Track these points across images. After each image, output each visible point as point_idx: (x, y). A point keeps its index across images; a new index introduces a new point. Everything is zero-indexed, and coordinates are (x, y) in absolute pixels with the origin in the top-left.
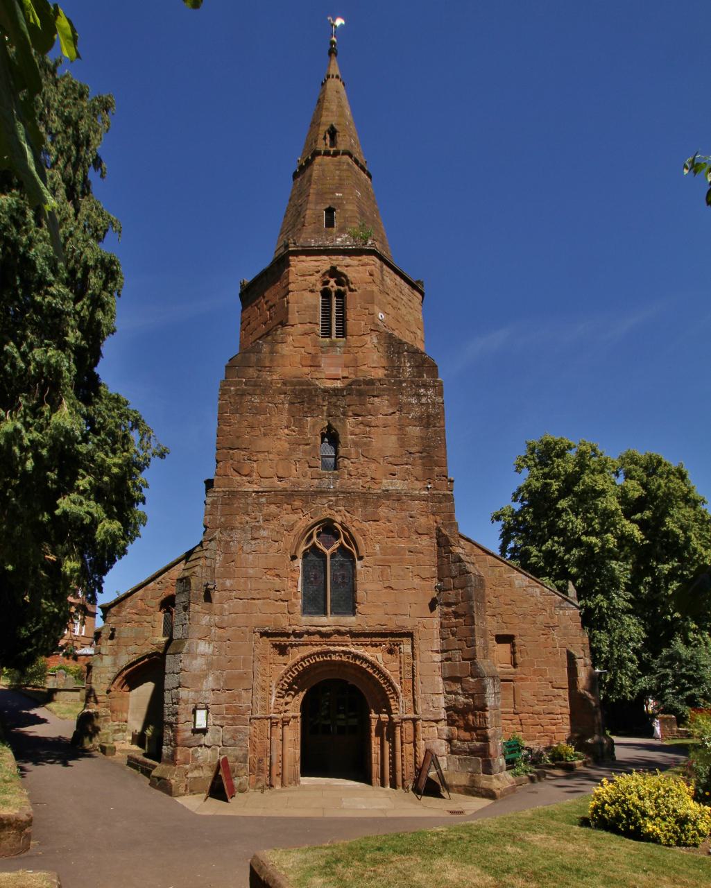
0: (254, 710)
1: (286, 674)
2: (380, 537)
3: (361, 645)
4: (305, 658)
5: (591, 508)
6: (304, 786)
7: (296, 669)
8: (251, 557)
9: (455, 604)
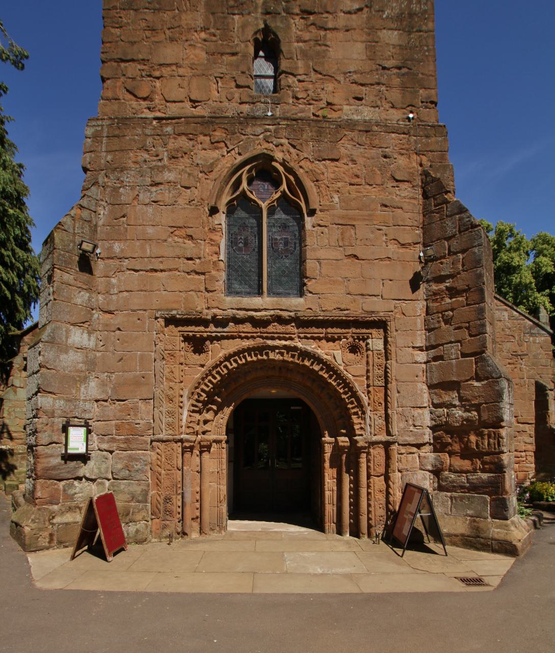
0: (157, 429)
1: (203, 379)
2: (339, 184)
3: (313, 338)
5: (505, 284)
6: (232, 533)
7: (218, 373)
8: (150, 210)
9: (451, 276)
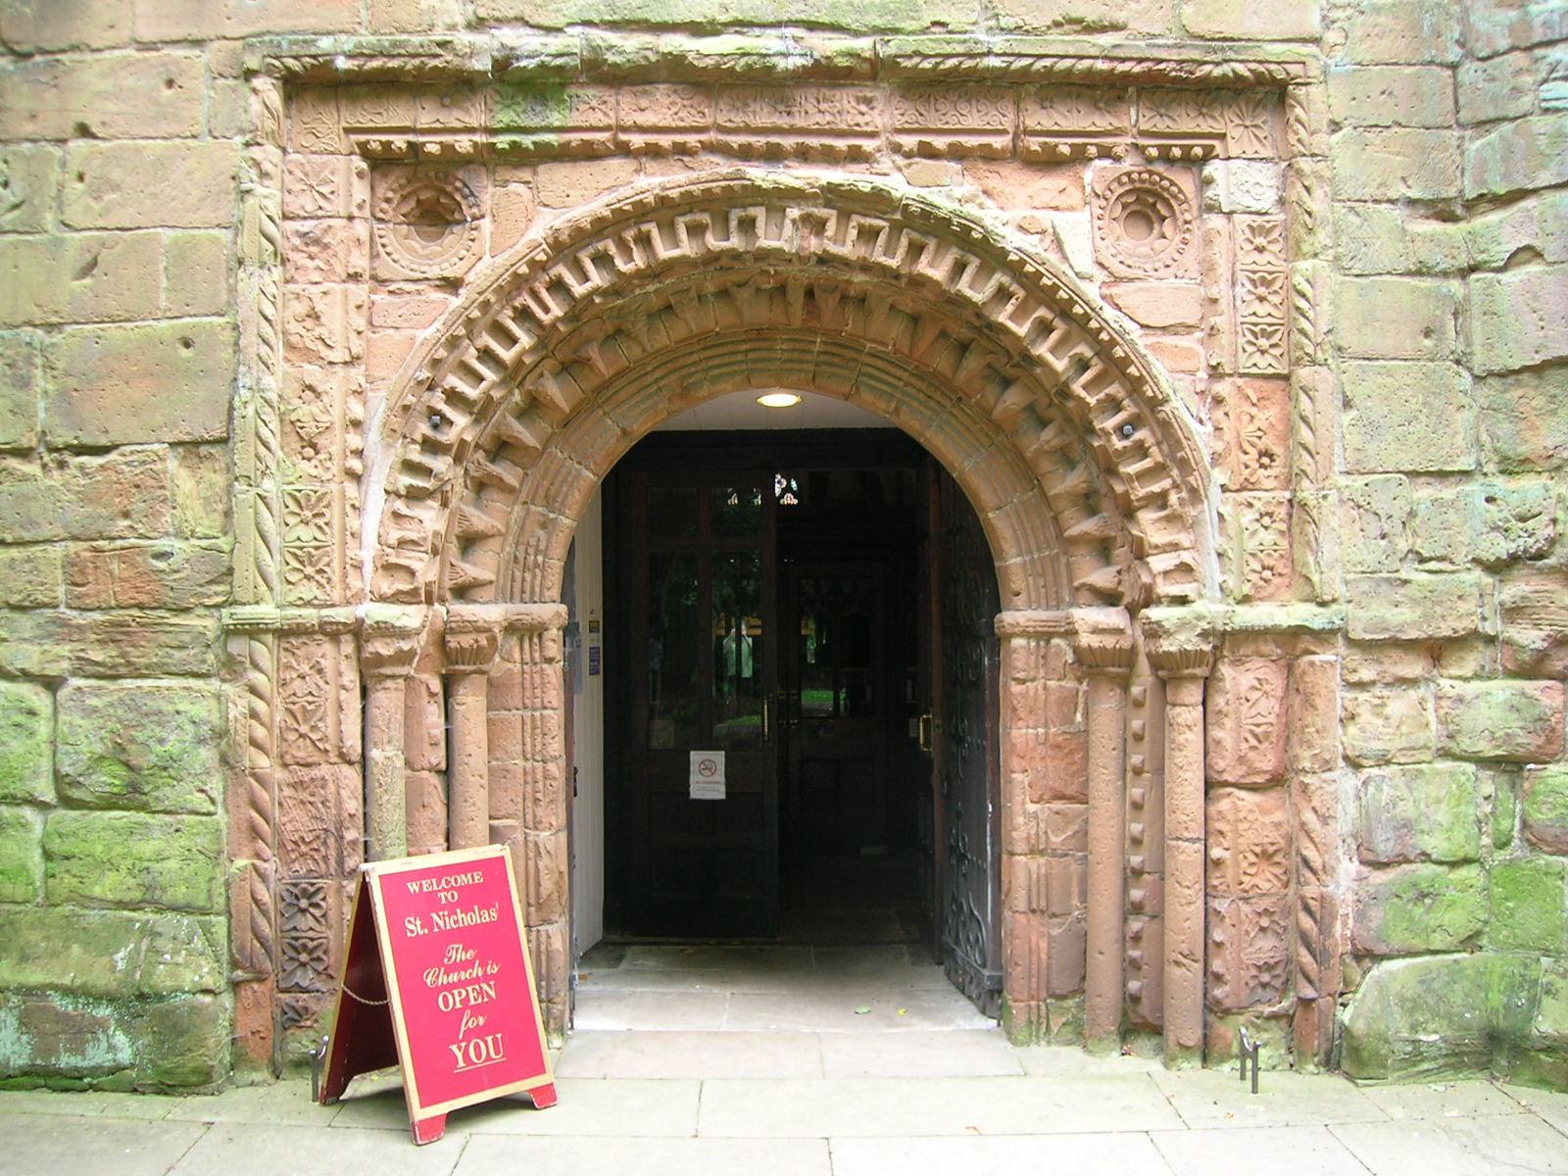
1: (453, 343)
3: (958, 154)
4: (581, 236)
7: (523, 315)
